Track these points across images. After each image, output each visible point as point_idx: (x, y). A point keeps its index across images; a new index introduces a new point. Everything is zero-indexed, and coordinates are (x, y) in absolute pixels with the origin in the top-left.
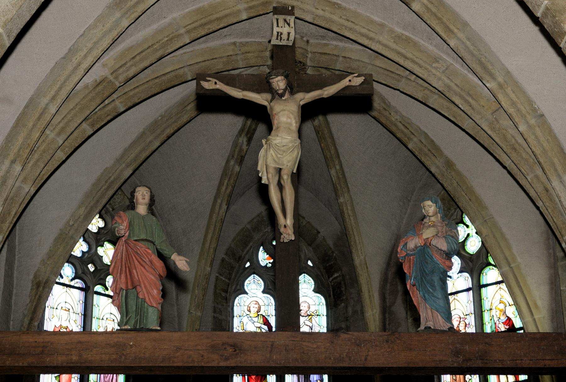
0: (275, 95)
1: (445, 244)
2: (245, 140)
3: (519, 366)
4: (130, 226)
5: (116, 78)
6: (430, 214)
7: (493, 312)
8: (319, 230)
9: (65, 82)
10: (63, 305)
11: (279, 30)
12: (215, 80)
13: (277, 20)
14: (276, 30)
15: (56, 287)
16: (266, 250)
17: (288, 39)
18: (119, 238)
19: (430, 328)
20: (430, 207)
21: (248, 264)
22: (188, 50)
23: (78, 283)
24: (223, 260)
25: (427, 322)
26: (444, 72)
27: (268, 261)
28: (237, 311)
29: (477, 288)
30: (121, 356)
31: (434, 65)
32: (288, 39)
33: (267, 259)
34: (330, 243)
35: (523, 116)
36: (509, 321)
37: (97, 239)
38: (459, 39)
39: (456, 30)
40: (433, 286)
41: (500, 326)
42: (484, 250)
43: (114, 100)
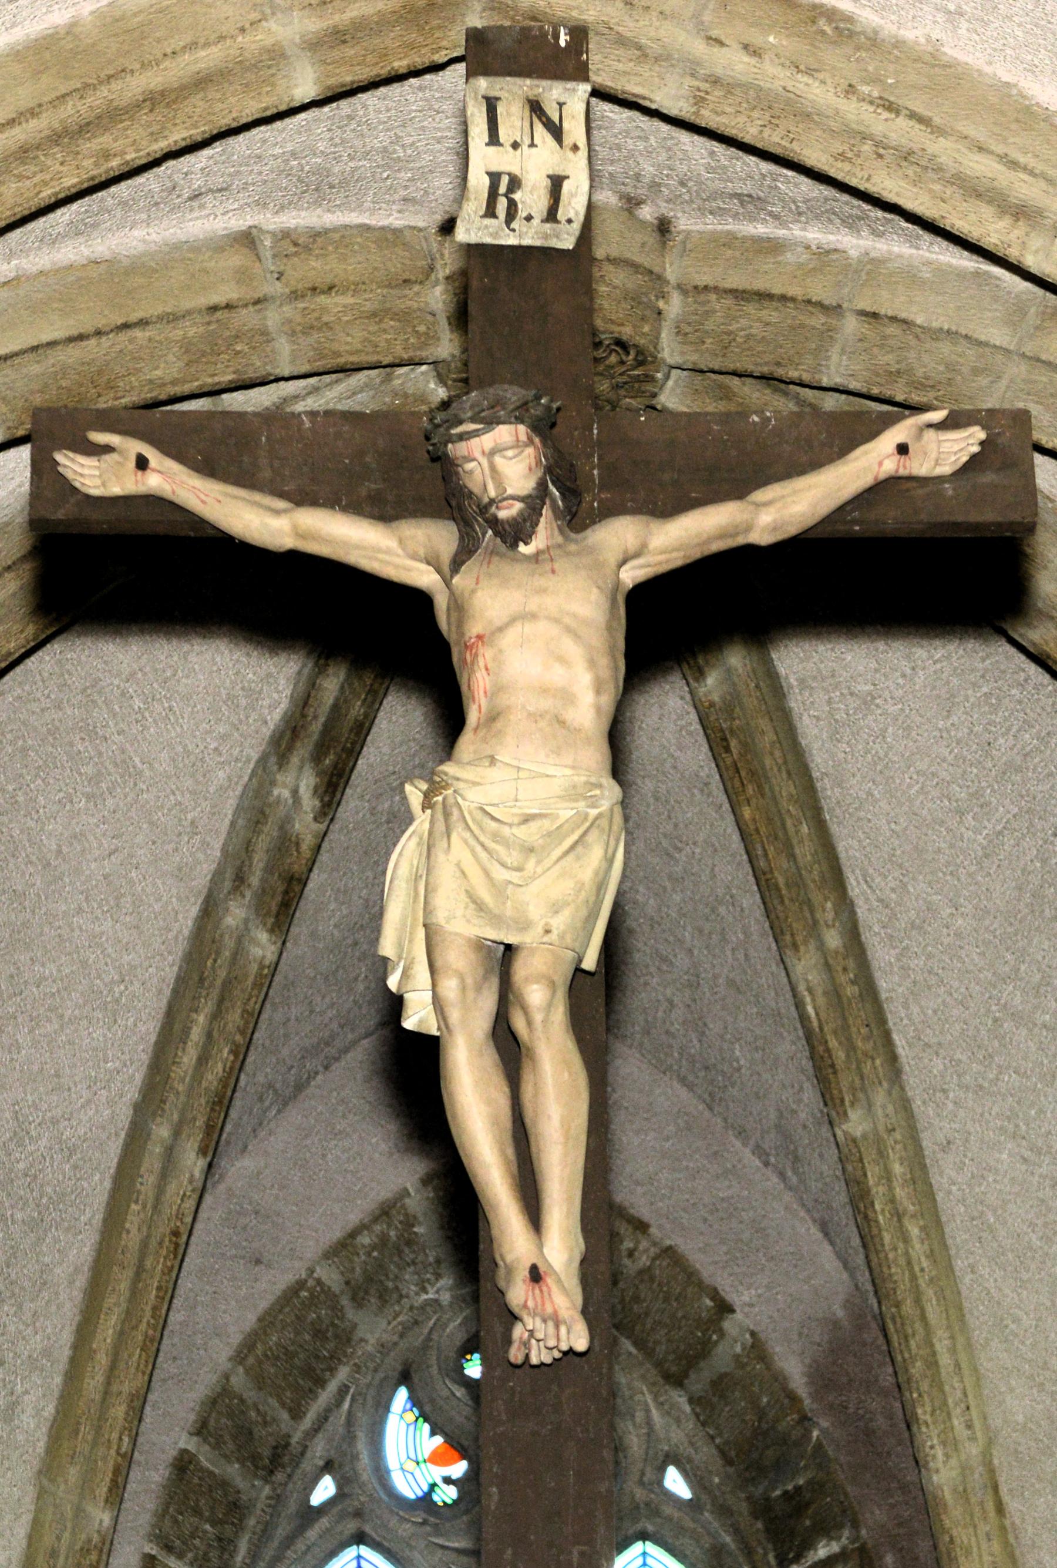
0: (481, 529)
11: (504, 160)
12: (136, 447)
13: (491, 105)
14: (484, 159)
17: (551, 215)
21: (324, 1490)
24: (183, 1464)
27: (437, 1473)
32: (551, 215)
33: (436, 1458)
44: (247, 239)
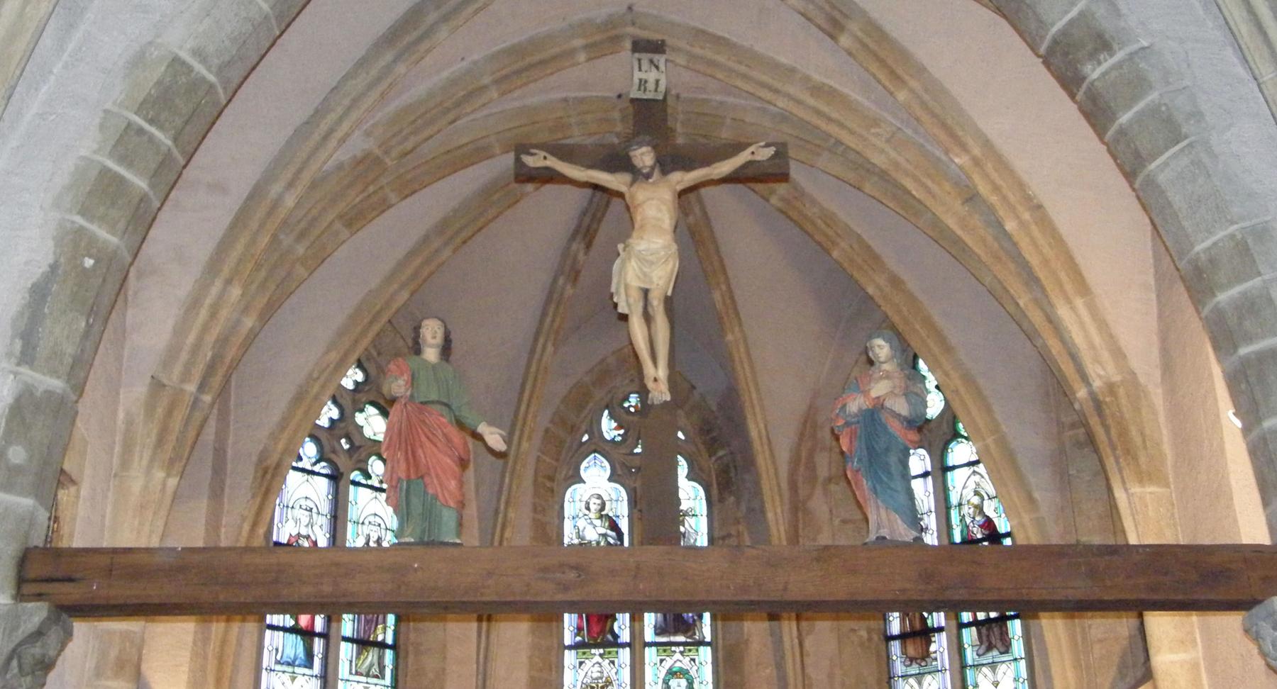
1: (906, 405)
2: (583, 246)
3: (1026, 598)
4: (413, 380)
5: (387, 152)
6: (882, 359)
7: (965, 510)
8: (694, 382)
9: (309, 158)
10: (303, 502)
11: (643, 76)
12: (543, 154)
13: (639, 60)
15: (293, 477)
16: (612, 416)
17: (656, 90)
18: (392, 401)
19: (884, 538)
20: (881, 348)
21: (586, 438)
22: (494, 110)
23: (322, 467)
24: (547, 431)
25: (879, 528)
26: (888, 141)
27: (616, 433)
28: (569, 510)
29: (942, 469)
30: (399, 587)
31: (873, 130)
32: (656, 90)
33: (616, 429)
35: (1012, 209)
36: (989, 524)
37: (350, 403)
38: (912, 91)
39: (906, 78)
40: (889, 473)
41: (975, 530)
42: (949, 416)
43: (381, 188)
44: (565, 100)
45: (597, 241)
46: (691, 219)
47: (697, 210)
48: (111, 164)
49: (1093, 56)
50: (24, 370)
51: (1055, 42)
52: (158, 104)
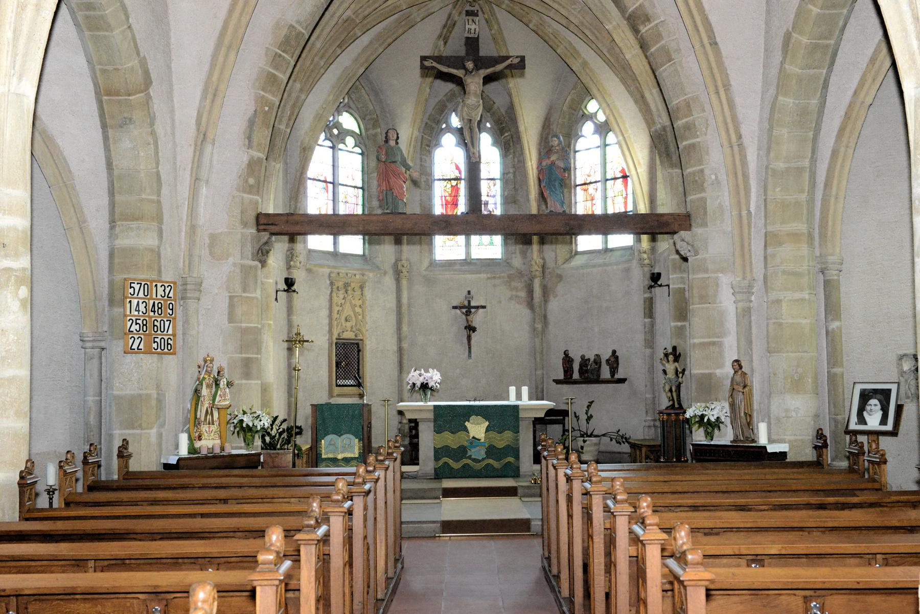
0: (467, 72)
5: (357, 16)
14: (467, 26)
21: (444, 126)
34: (503, 111)
45: (450, 41)
46: (493, 32)
47: (496, 27)
48: (270, 70)
49: (643, 23)
50: (250, 151)
51: (630, 15)
52: (285, 44)
